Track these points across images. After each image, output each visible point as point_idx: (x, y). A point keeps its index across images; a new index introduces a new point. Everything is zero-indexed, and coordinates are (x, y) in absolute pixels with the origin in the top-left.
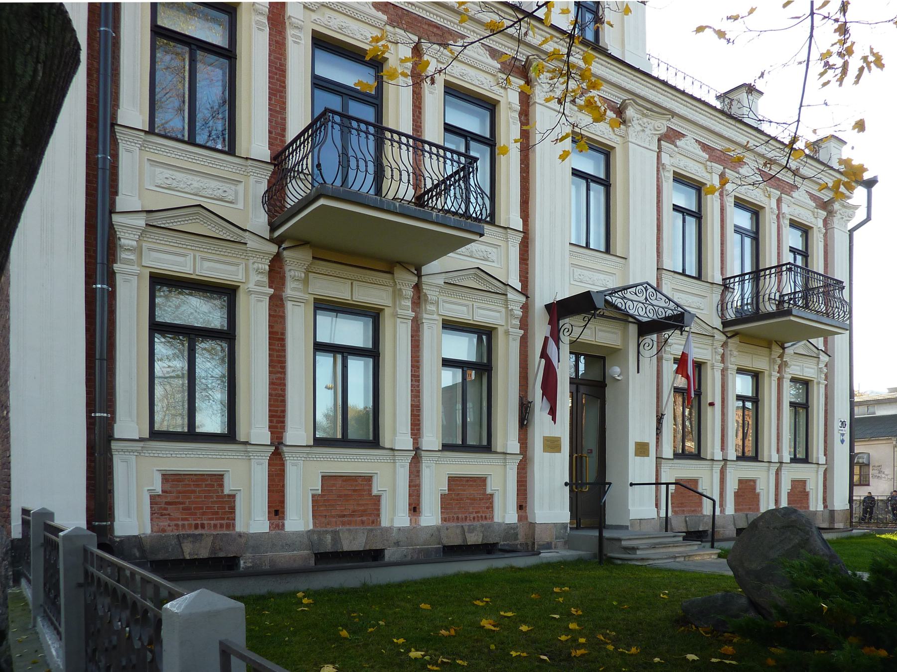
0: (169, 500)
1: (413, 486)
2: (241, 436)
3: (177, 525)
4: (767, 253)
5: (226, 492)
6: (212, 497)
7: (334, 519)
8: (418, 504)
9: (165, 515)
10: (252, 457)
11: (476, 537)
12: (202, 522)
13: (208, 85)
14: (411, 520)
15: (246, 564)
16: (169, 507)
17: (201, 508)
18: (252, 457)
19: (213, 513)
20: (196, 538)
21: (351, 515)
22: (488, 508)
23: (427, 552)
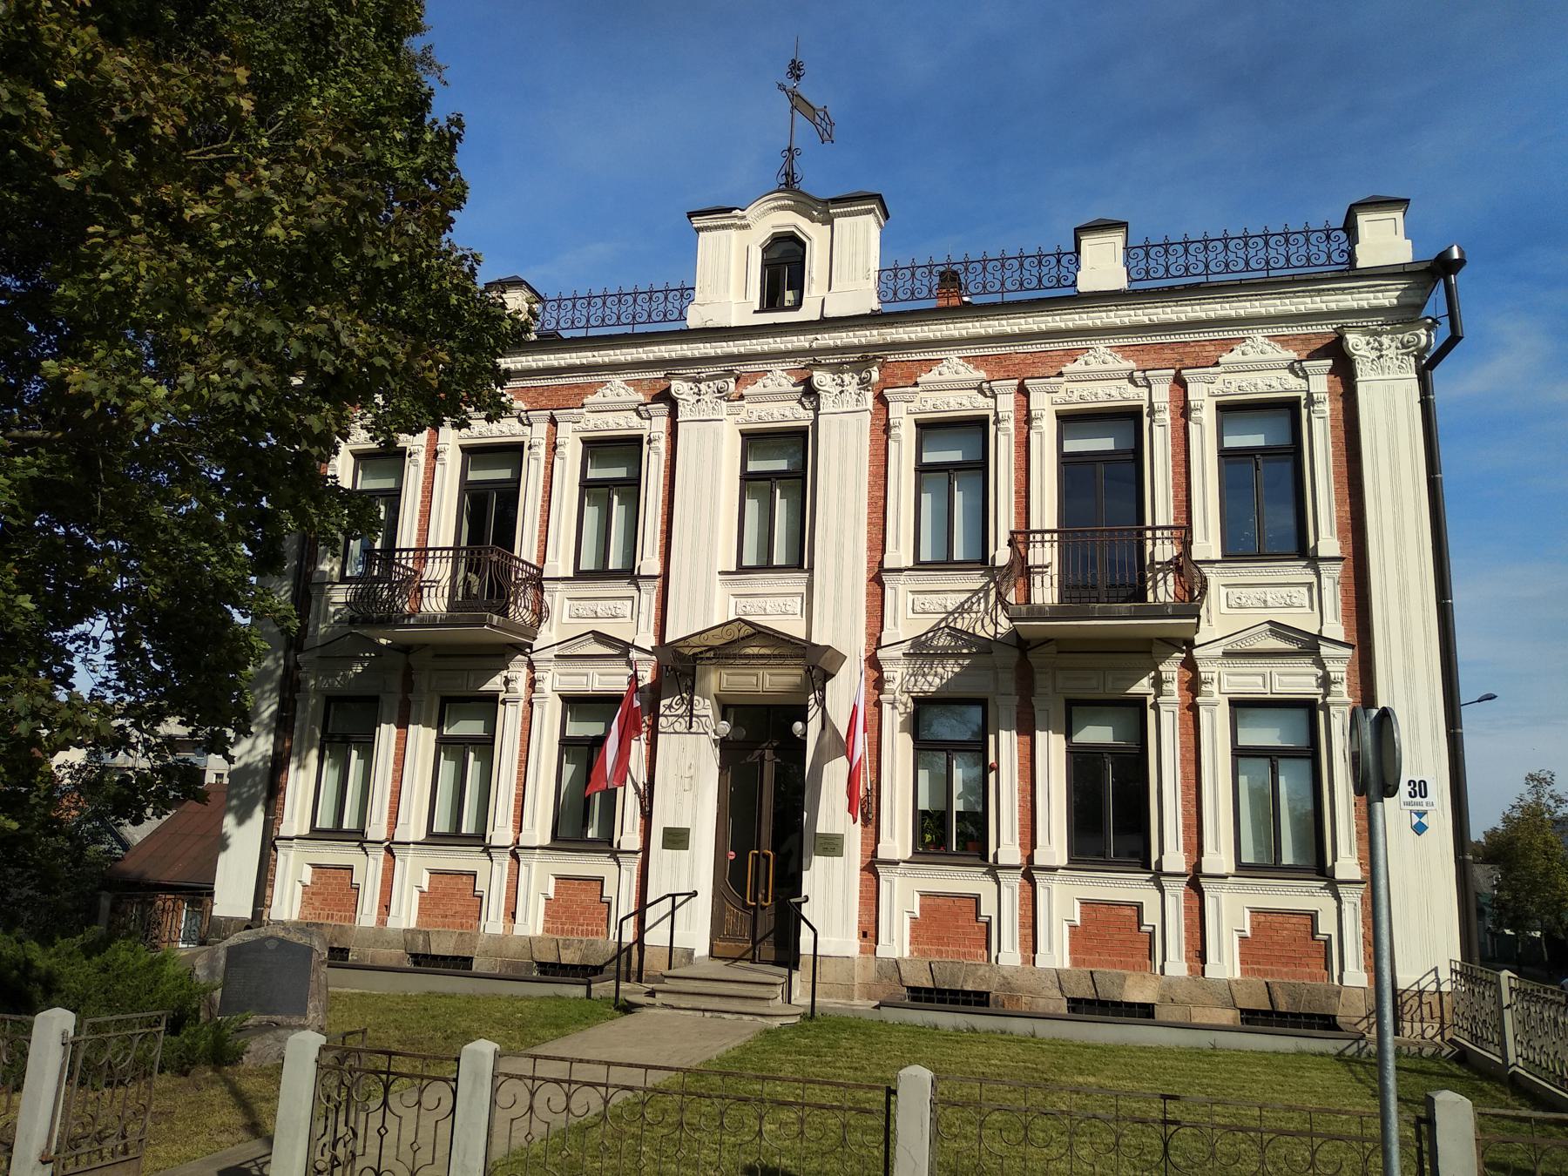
23: (515, 966)
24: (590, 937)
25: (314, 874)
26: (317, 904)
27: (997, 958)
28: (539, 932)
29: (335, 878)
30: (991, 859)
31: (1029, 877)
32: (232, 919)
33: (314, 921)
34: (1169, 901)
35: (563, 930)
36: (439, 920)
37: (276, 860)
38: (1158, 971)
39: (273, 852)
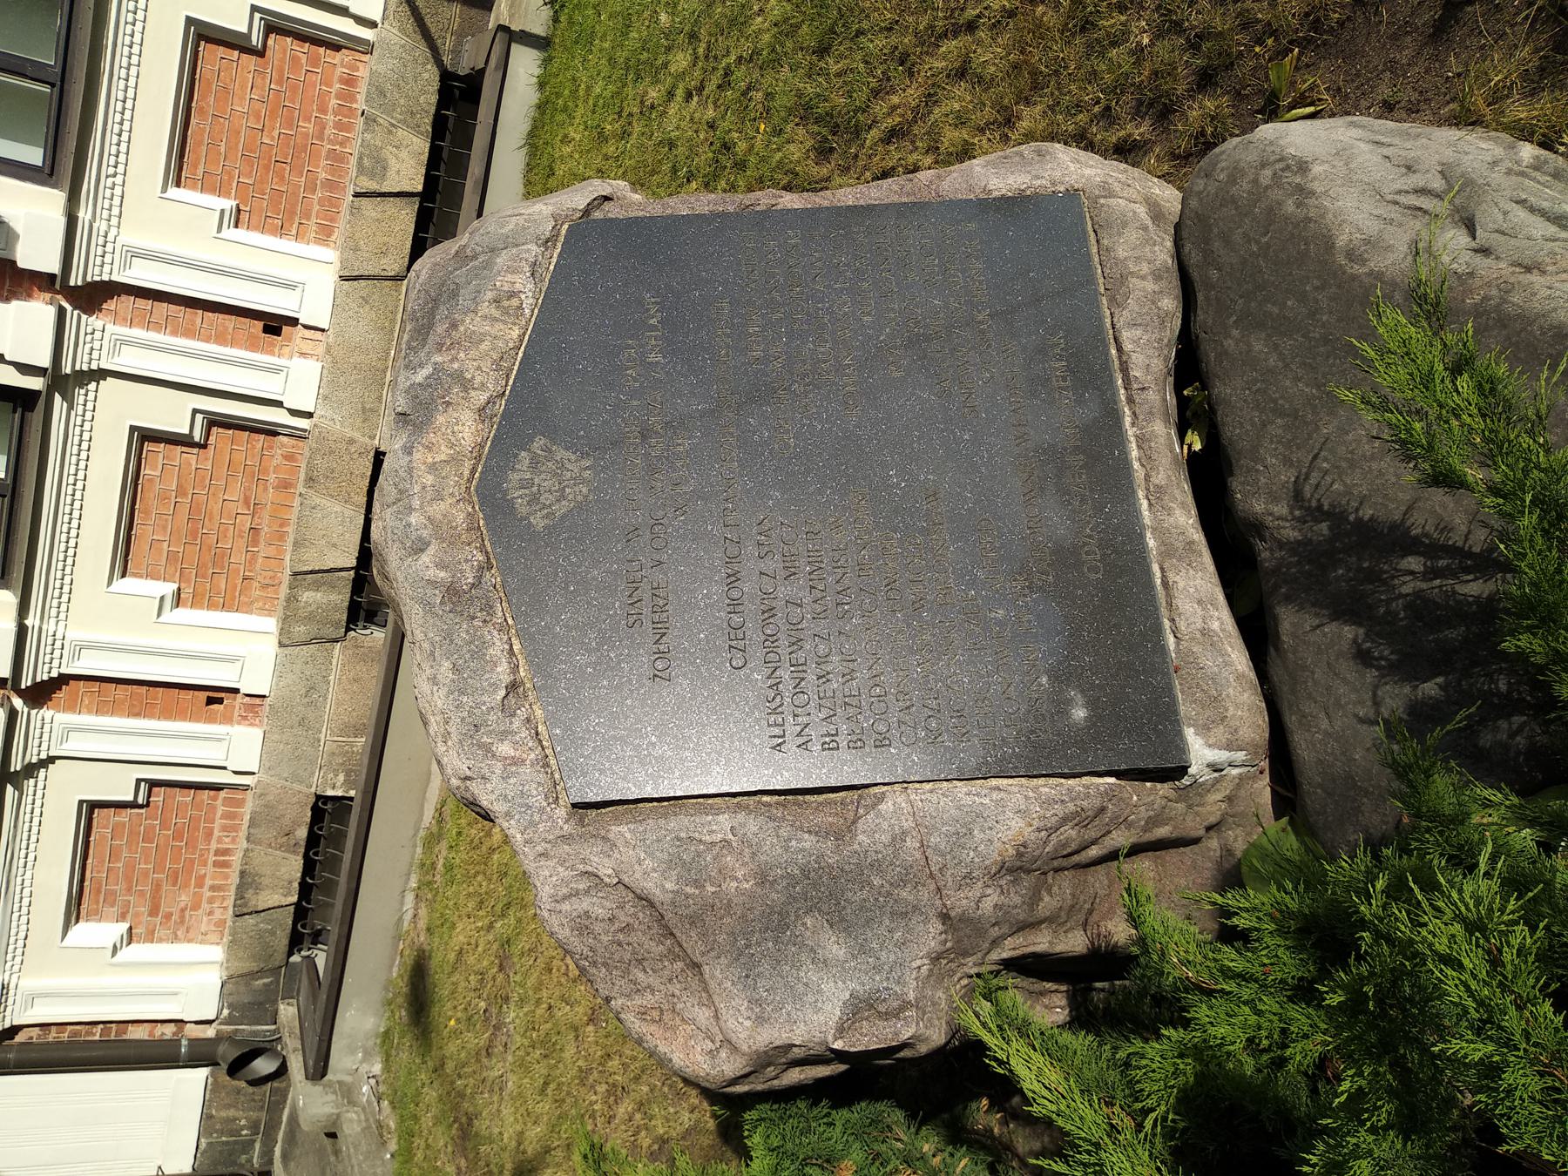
0: (144, 910)
4: (89, 160)
11: (404, 154)
12: (212, 852)
13: (713, 411)
14: (303, 354)
15: (338, 784)
16: (163, 909)
20: (247, 881)
25: (96, 915)
26: (184, 899)
27: (295, 413)
28: (330, 254)
29: (114, 854)
30: (35, 383)
31: (94, 296)
32: (206, 1118)
33: (230, 902)
34: (129, 361)
36: (263, 550)
37: (44, 1026)
38: (303, 423)
39: (20, 1038)
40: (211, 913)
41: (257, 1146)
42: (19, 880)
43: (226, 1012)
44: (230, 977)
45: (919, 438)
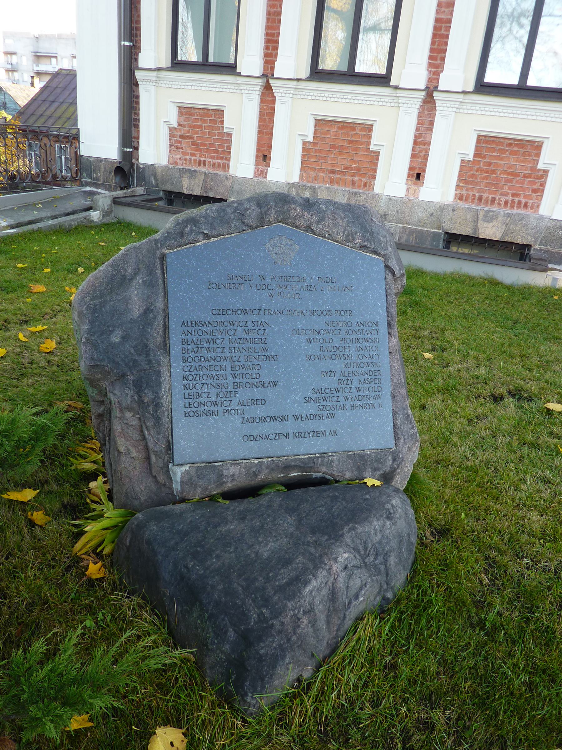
0: (182, 133)
1: (421, 143)
2: (393, 81)
3: (186, 159)
5: (540, 166)
6: (214, 134)
7: (323, 175)
8: (424, 171)
9: (179, 148)
10: (243, 91)
12: (205, 159)
14: (408, 190)
17: (205, 145)
18: (243, 91)
19: (217, 152)
20: (193, 174)
21: (342, 173)
22: (534, 191)
23: (420, 235)
24: (508, 210)
32: (101, 160)
35: (480, 199)
40: (180, 159)
41: (89, 180)
42: (194, 84)
43: (142, 166)
44: (155, 168)
45: (297, 381)
